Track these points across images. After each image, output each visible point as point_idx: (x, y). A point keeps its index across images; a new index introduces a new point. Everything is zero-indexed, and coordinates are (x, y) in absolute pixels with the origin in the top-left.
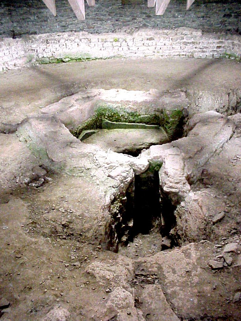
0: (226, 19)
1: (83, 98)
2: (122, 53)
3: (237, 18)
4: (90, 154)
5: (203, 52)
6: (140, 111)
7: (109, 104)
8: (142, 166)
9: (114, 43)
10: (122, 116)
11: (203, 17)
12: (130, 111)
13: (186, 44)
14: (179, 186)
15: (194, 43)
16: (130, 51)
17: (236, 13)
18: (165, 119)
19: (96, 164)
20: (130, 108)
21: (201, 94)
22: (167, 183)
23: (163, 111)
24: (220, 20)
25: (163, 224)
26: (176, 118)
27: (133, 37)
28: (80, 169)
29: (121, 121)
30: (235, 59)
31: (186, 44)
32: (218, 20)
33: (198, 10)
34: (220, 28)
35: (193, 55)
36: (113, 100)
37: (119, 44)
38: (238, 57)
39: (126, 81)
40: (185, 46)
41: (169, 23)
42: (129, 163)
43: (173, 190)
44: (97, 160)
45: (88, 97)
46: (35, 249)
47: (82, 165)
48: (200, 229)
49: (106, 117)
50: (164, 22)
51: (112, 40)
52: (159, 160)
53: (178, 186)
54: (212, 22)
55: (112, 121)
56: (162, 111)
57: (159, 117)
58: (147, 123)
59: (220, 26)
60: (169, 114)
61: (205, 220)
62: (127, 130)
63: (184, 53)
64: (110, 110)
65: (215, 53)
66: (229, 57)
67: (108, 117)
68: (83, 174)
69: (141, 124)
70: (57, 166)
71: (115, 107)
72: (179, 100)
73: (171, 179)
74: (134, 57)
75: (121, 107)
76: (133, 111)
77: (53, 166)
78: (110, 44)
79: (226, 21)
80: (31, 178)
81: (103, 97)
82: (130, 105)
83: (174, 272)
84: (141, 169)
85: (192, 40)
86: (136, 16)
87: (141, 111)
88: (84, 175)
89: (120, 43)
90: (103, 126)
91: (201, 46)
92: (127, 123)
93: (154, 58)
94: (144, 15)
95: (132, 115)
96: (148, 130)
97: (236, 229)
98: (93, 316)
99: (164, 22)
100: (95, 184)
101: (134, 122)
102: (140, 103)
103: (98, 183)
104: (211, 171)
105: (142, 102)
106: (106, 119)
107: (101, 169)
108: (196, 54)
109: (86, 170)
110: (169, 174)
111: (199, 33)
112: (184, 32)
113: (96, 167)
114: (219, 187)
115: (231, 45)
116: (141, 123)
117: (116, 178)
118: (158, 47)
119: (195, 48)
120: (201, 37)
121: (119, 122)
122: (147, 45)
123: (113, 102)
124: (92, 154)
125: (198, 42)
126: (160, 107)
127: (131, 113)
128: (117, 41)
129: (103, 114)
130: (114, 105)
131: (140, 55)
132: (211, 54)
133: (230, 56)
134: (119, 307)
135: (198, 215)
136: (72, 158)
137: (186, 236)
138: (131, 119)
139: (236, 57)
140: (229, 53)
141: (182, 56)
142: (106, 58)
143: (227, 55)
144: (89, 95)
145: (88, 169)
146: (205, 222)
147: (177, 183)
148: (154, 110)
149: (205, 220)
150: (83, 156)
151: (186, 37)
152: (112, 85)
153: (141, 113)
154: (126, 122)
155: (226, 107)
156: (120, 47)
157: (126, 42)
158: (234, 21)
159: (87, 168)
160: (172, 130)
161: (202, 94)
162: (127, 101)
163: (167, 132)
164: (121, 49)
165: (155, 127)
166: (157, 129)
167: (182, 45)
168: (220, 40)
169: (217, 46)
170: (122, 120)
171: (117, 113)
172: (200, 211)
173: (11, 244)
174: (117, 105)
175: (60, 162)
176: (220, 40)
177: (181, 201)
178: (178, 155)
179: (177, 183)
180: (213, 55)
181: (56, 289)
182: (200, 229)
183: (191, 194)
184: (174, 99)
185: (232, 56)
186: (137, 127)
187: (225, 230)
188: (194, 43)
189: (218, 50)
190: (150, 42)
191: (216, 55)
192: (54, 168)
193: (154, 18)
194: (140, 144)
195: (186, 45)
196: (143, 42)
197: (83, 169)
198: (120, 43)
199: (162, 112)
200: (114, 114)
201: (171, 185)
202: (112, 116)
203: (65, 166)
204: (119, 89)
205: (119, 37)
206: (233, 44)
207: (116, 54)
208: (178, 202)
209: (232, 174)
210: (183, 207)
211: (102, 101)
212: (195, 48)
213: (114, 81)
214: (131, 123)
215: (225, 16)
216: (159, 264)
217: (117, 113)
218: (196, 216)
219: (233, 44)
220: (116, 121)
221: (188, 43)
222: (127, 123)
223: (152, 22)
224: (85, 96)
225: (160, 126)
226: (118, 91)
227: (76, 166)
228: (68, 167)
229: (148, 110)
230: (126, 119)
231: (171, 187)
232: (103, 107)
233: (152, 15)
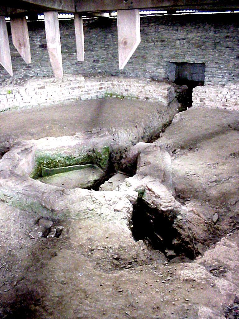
0: (95, 64)
1: (22, 151)
2: (16, 104)
3: (103, 63)
4: (88, 196)
5: (89, 94)
6: (74, 154)
7: (46, 152)
8: (135, 196)
9: (8, 95)
10: (59, 161)
11: (77, 64)
12: (65, 156)
13: (73, 89)
14: (171, 204)
15: (80, 87)
16: (24, 101)
17: (103, 58)
18: (98, 157)
19: (98, 204)
20: (66, 152)
21: (114, 130)
22: (162, 204)
23: (95, 149)
24: (90, 66)
25: (162, 240)
26: (106, 154)
27: (25, 88)
28: (84, 211)
29: (58, 167)
30: (117, 97)
31: (73, 89)
32: (89, 65)
33: (72, 58)
34: (92, 72)
35: (80, 98)
36: (48, 148)
37: (12, 96)
38: (119, 95)
39: (44, 129)
40: (73, 91)
41: (47, 71)
42: (126, 195)
43: (170, 208)
44: (97, 200)
45: (26, 149)
46: (127, 280)
47: (86, 208)
48: (205, 231)
49: (45, 165)
50: (43, 72)
51: (6, 93)
52: (141, 188)
53: (171, 204)
54: (84, 68)
55: (51, 168)
56: (94, 150)
57: (92, 156)
58: (81, 164)
59: (92, 70)
60: (101, 152)
61: (206, 223)
62: (66, 174)
63: (73, 97)
64: (48, 158)
65: (98, 94)
66: (111, 95)
67: (47, 164)
68: (89, 215)
69: (77, 166)
70: (60, 215)
71: (52, 154)
72: (106, 138)
73: (164, 200)
74: (29, 106)
75: (57, 153)
76: (68, 155)
77: (56, 215)
78: (4, 97)
79: (96, 65)
80: (42, 232)
81: (39, 147)
82: (65, 150)
83: (231, 260)
84: (134, 199)
85: (78, 85)
86: (17, 68)
87: (75, 154)
88: (91, 216)
89: (13, 95)
90: (43, 174)
91: (86, 89)
92: (64, 167)
93: (47, 105)
94: (24, 67)
95: (69, 158)
96: (84, 170)
97: (233, 222)
98: (221, 304)
99: (43, 72)
100: (107, 220)
101: (70, 165)
102: (73, 147)
103: (110, 218)
104: (180, 188)
105: (75, 146)
106: (45, 167)
107: (105, 206)
108: (83, 96)
109: (91, 211)
110: (161, 197)
111: (83, 78)
112: (69, 79)
113: (99, 206)
114: (196, 197)
115: (111, 86)
116: (76, 164)
117: (122, 211)
118: (49, 96)
119: (82, 91)
120: (85, 81)
121: (57, 167)
122: (39, 94)
123: (50, 150)
124: (89, 196)
125: (83, 86)
126: (91, 148)
127: (67, 157)
128: (11, 93)
129: (42, 163)
130: (50, 152)
131: (34, 103)
132: (96, 95)
133: (111, 95)
134: (232, 290)
135: (199, 221)
136: (73, 203)
137: (195, 239)
138: (68, 162)
139: (117, 96)
140: (110, 92)
141: (71, 100)
142: (2, 110)
143: (109, 94)
144: (26, 147)
145: (92, 210)
146: (206, 225)
147: (170, 202)
148: (86, 150)
149: (206, 223)
150: (82, 199)
151: (73, 83)
152: (48, 134)
153: (75, 156)
154: (63, 167)
155: (137, 137)
156: (14, 98)
157: (19, 93)
158: (102, 65)
159: (91, 208)
160: (106, 165)
161: (116, 130)
162: (62, 147)
163: (102, 168)
164: (15, 100)
165: (90, 165)
166: (92, 167)
167: (71, 91)
168: (101, 82)
169: (99, 88)
170: (60, 165)
171: (54, 159)
172: (199, 217)
173: (103, 284)
174: (54, 152)
175: (62, 210)
176: (101, 82)
177: (178, 215)
178: (154, 181)
179: (170, 202)
180: (97, 96)
181: (179, 299)
182: (205, 231)
183: (184, 207)
184: (102, 138)
185: (114, 95)
186: (73, 169)
187: (226, 225)
188: (80, 87)
189: (100, 91)
190: (41, 91)
191: (99, 95)
192: (57, 217)
193: (34, 68)
194: (86, 183)
195: (73, 89)
196: (35, 91)
197: (87, 210)
198: (13, 95)
199: (94, 151)
200: (52, 160)
201: (166, 204)
202: (50, 163)
203: (69, 212)
204: (48, 137)
205: (12, 89)
206: (112, 84)
207: (11, 106)
208: (175, 217)
209: (195, 187)
210: (181, 219)
211: (39, 150)
212: (82, 91)
213: (34, 130)
214: (67, 166)
215: (94, 61)
216: (216, 259)
217: (54, 159)
218: (197, 223)
219: (112, 84)
220: (55, 167)
221: (75, 88)
222: (64, 167)
223: (32, 72)
224: (23, 148)
225: (93, 164)
226: (47, 140)
227: (80, 209)
228: (73, 213)
229: (81, 152)
230: (62, 163)
231: (167, 207)
232: (41, 156)
233: (31, 66)
